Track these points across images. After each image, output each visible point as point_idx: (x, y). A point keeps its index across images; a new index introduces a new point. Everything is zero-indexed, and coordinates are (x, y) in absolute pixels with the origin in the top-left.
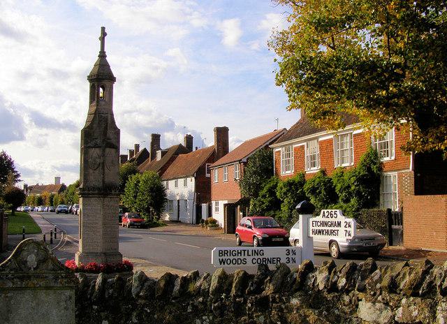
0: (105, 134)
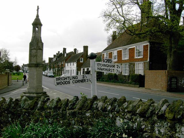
0: (37, 44)
